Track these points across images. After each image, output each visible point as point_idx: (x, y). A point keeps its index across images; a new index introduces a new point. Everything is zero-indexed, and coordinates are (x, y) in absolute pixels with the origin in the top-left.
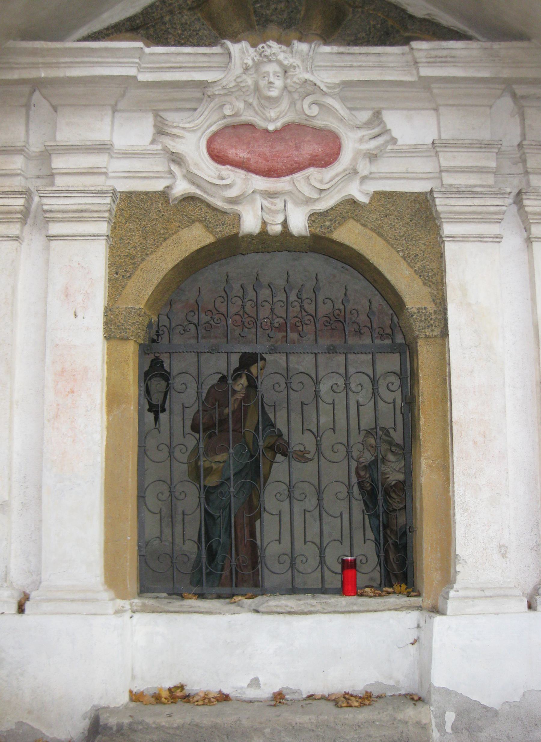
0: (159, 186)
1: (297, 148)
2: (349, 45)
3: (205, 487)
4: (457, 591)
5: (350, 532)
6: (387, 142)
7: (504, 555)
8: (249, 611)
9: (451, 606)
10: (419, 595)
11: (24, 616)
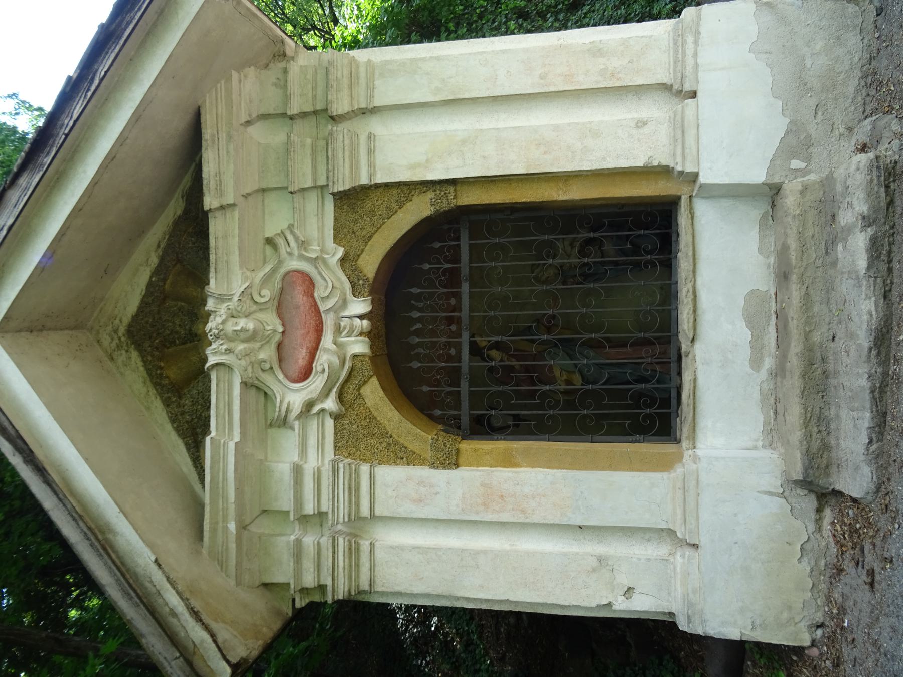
0: (329, 423)
1: (298, 307)
2: (208, 265)
3: (582, 385)
4: (677, 164)
5: (164, 630)
6: (292, 232)
7: (645, 124)
8: (692, 346)
9: (690, 168)
10: (679, 198)
11: (701, 544)
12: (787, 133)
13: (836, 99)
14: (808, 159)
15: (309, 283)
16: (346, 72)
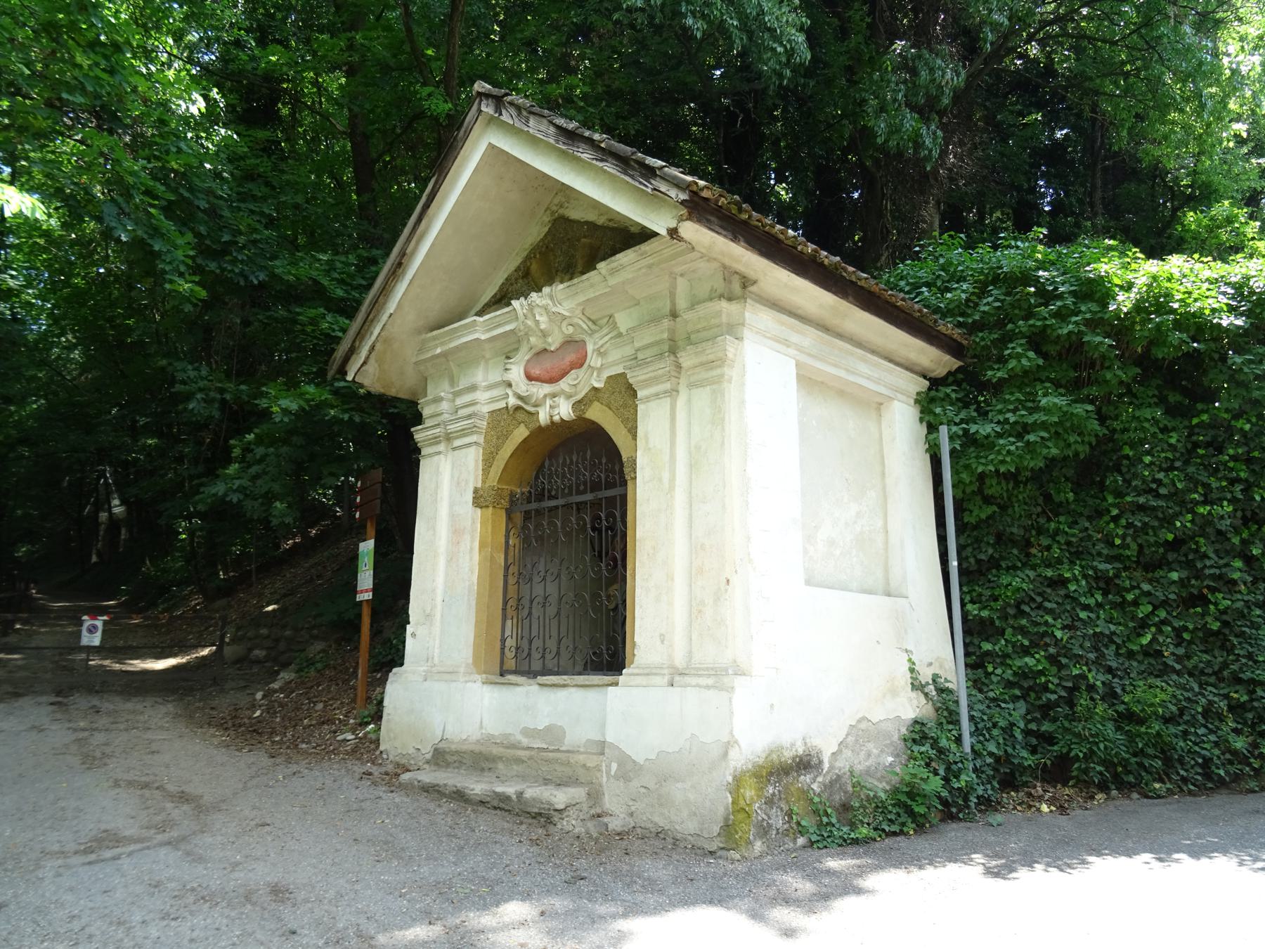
12: (634, 762)
13: (652, 806)
14: (617, 777)
15: (579, 363)
16: (711, 357)
